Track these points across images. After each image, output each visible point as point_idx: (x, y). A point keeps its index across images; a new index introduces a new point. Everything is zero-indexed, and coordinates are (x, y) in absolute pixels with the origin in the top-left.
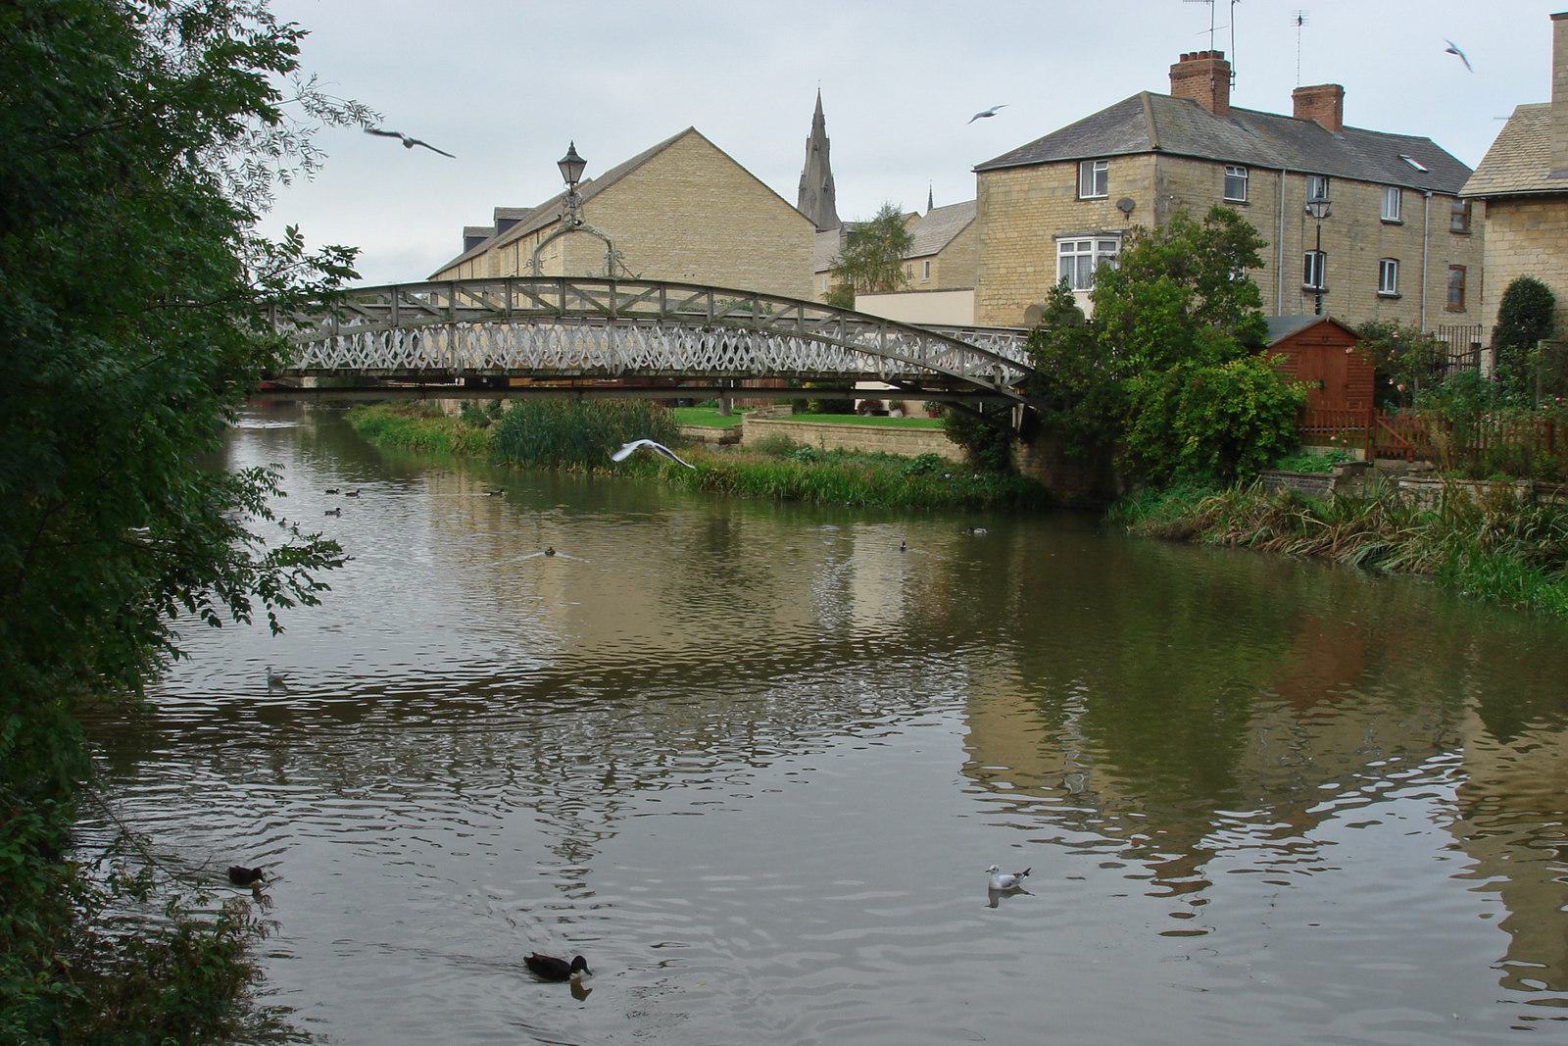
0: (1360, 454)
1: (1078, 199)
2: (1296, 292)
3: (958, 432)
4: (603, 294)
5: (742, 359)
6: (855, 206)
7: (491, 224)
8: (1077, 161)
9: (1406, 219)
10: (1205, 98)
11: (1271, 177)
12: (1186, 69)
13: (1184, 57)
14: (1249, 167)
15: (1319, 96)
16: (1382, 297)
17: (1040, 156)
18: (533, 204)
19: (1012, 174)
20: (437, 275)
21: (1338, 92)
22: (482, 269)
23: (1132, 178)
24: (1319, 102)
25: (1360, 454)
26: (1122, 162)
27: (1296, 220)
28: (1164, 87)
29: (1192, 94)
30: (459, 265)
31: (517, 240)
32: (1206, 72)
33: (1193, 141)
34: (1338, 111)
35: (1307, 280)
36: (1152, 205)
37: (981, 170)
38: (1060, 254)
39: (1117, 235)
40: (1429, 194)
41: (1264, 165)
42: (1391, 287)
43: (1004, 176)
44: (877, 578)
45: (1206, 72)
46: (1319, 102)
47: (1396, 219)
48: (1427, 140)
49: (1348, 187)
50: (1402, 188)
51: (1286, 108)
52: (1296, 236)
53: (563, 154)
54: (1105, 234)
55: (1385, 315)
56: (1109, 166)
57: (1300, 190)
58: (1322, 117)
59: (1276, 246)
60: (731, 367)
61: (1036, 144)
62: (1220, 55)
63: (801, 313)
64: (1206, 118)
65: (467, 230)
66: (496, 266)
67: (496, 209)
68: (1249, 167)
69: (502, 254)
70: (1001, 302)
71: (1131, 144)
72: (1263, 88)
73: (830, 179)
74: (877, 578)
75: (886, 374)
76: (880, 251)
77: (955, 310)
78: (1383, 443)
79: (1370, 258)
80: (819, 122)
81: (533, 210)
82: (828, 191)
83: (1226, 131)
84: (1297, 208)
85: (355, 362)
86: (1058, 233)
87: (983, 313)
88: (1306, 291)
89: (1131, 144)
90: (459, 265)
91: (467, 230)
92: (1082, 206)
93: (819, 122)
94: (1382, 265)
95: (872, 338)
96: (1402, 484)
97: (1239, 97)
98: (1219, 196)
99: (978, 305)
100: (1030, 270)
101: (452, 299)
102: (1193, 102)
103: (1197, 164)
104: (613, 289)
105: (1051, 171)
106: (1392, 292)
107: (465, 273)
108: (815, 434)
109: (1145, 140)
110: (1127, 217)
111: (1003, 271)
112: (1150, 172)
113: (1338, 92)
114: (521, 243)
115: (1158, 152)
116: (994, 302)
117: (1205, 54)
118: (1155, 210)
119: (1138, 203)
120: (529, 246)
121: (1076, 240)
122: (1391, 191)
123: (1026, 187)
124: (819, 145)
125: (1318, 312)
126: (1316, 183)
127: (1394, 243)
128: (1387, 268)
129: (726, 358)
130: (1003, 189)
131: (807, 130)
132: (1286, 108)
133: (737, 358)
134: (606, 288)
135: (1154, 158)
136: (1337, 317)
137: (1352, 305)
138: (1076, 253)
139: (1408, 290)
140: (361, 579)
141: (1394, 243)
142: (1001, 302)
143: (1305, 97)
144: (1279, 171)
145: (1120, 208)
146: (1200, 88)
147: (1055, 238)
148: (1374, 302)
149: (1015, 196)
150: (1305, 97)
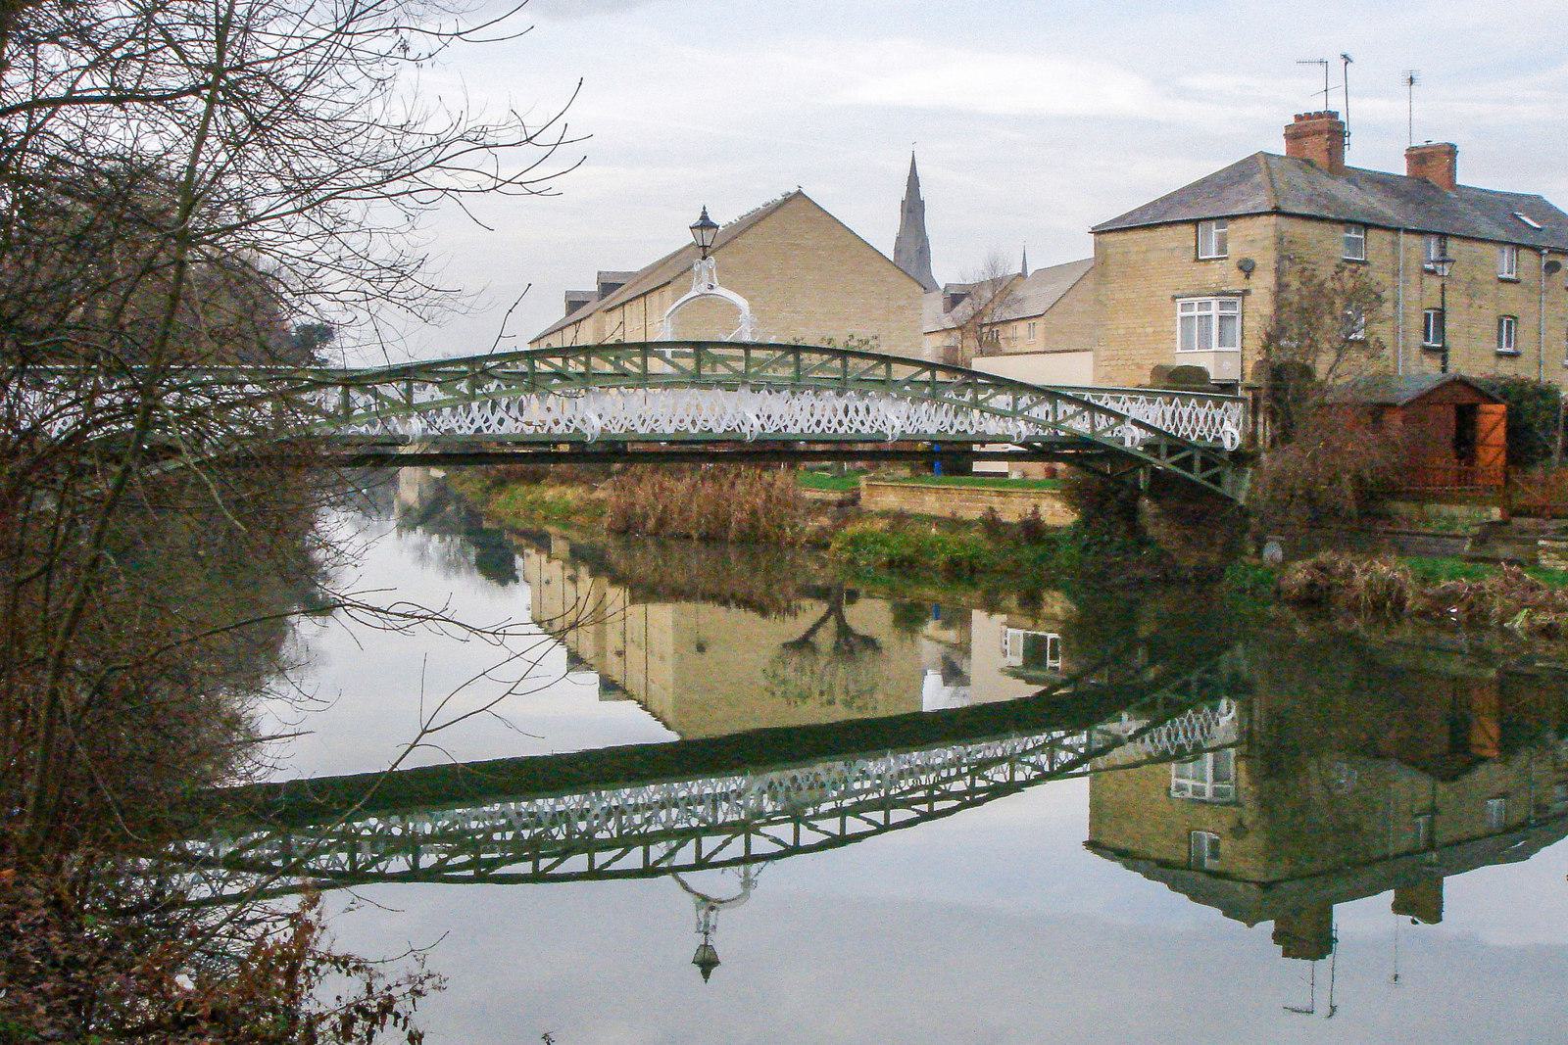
0: (1496, 513)
1: (1197, 260)
2: (1415, 351)
3: (1074, 495)
4: (739, 359)
5: (829, 422)
6: (946, 271)
7: (595, 288)
8: (1196, 222)
9: (1522, 277)
10: (1320, 158)
11: (1388, 236)
12: (1299, 132)
13: (1298, 118)
14: (1367, 226)
15: (1432, 155)
16: (1500, 355)
17: (1155, 218)
18: (636, 266)
19: (1131, 235)
20: (538, 339)
21: (1451, 151)
22: (587, 336)
23: (1255, 238)
24: (1432, 163)
25: (1496, 513)
26: (1241, 223)
27: (1414, 279)
28: (1280, 147)
29: (1308, 154)
30: (561, 329)
31: (623, 304)
32: (1320, 133)
33: (1310, 200)
34: (1452, 170)
35: (1427, 338)
36: (1273, 266)
37: (1098, 232)
38: (1180, 314)
39: (1238, 295)
40: (1545, 251)
41: (1381, 223)
42: (1509, 344)
43: (1121, 237)
44: (999, 652)
45: (1320, 135)
46: (1432, 163)
47: (1512, 276)
48: (1539, 197)
49: (1466, 246)
50: (1518, 246)
51: (1401, 169)
52: (1414, 294)
53: (696, 219)
54: (1224, 294)
55: (1507, 369)
56: (1232, 226)
57: (1418, 250)
58: (1435, 176)
59: (1396, 304)
60: (818, 431)
61: (1153, 204)
62: (1335, 115)
63: (933, 376)
64: (1324, 179)
65: (568, 294)
66: (600, 330)
67: (599, 273)
68: (1367, 226)
69: (607, 318)
70: (1120, 362)
71: (1250, 204)
72: (1380, 149)
73: (925, 240)
74: (999, 652)
75: (1019, 437)
76: (986, 310)
77: (1075, 371)
78: (1519, 500)
79: (1490, 313)
80: (913, 182)
81: (636, 274)
82: (923, 252)
83: (1341, 190)
84: (1414, 265)
85: (460, 427)
86: (1177, 293)
87: (1102, 374)
88: (1427, 350)
89: (1250, 204)
90: (561, 329)
91: (568, 294)
92: (1201, 267)
93: (913, 182)
94: (1501, 322)
95: (1002, 401)
96: (1541, 543)
97: (1354, 157)
98: (1342, 253)
99: (1097, 366)
100: (1150, 330)
101: (587, 364)
102: (1308, 162)
103: (1315, 224)
104: (747, 354)
105: (1169, 232)
106: (1510, 350)
107: (567, 339)
108: (935, 500)
109: (1262, 201)
110: (1247, 277)
111: (1122, 331)
112: (1270, 232)
113: (1451, 151)
114: (627, 307)
115: (1277, 212)
116: (1113, 363)
117: (1319, 115)
118: (1277, 270)
119: (1259, 262)
120: (634, 311)
121: (1196, 300)
122: (1507, 249)
123: (1144, 248)
124: (913, 208)
125: (1444, 370)
126: (1433, 241)
127: (1513, 301)
128: (1507, 323)
129: (813, 421)
130: (1120, 250)
131: (902, 192)
132: (1401, 169)
133: (846, 421)
134: (741, 352)
135: (1273, 219)
136: (1464, 372)
137: (1474, 358)
138: (1196, 313)
139: (1526, 346)
140: (404, 651)
141: (1513, 301)
142: (1120, 362)
143: (1419, 157)
144: (1397, 230)
145: (1240, 268)
146: (1315, 149)
147: (1174, 298)
148: (1492, 360)
149: (1134, 257)
150: (1419, 157)
